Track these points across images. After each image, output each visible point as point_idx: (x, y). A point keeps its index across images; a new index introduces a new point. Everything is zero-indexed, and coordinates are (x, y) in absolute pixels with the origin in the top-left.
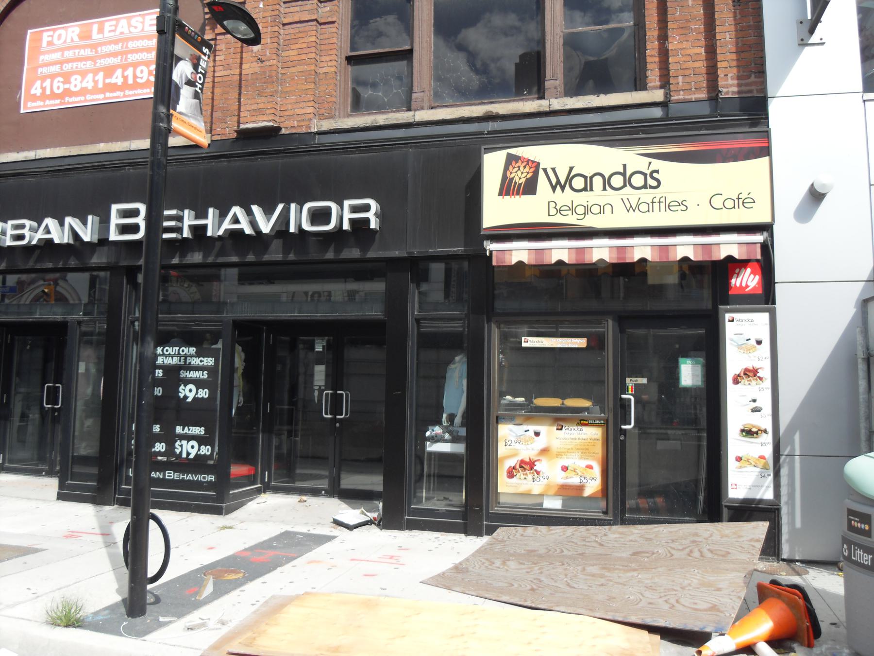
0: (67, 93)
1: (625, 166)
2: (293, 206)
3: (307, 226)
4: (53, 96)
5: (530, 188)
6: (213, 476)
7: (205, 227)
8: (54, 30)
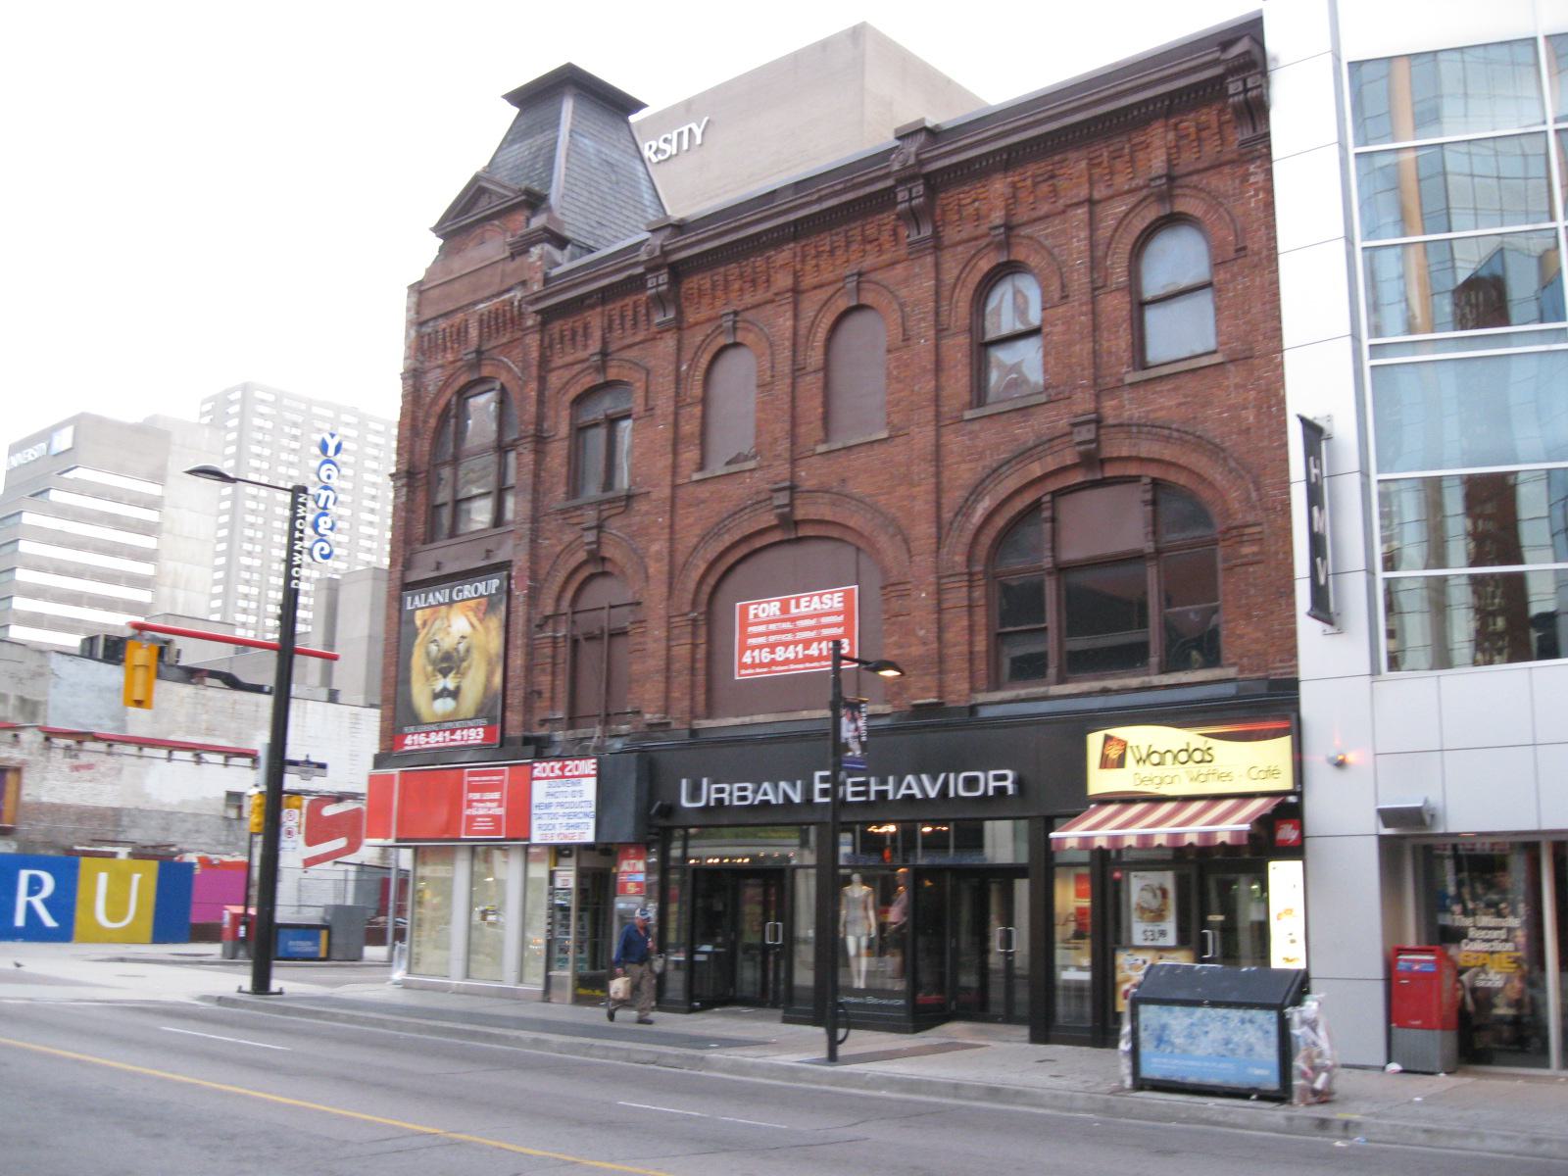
0: (773, 662)
1: (1188, 744)
2: (952, 776)
3: (963, 793)
4: (762, 665)
5: (1120, 763)
6: (1010, 773)
7: (886, 792)
8: (759, 604)
